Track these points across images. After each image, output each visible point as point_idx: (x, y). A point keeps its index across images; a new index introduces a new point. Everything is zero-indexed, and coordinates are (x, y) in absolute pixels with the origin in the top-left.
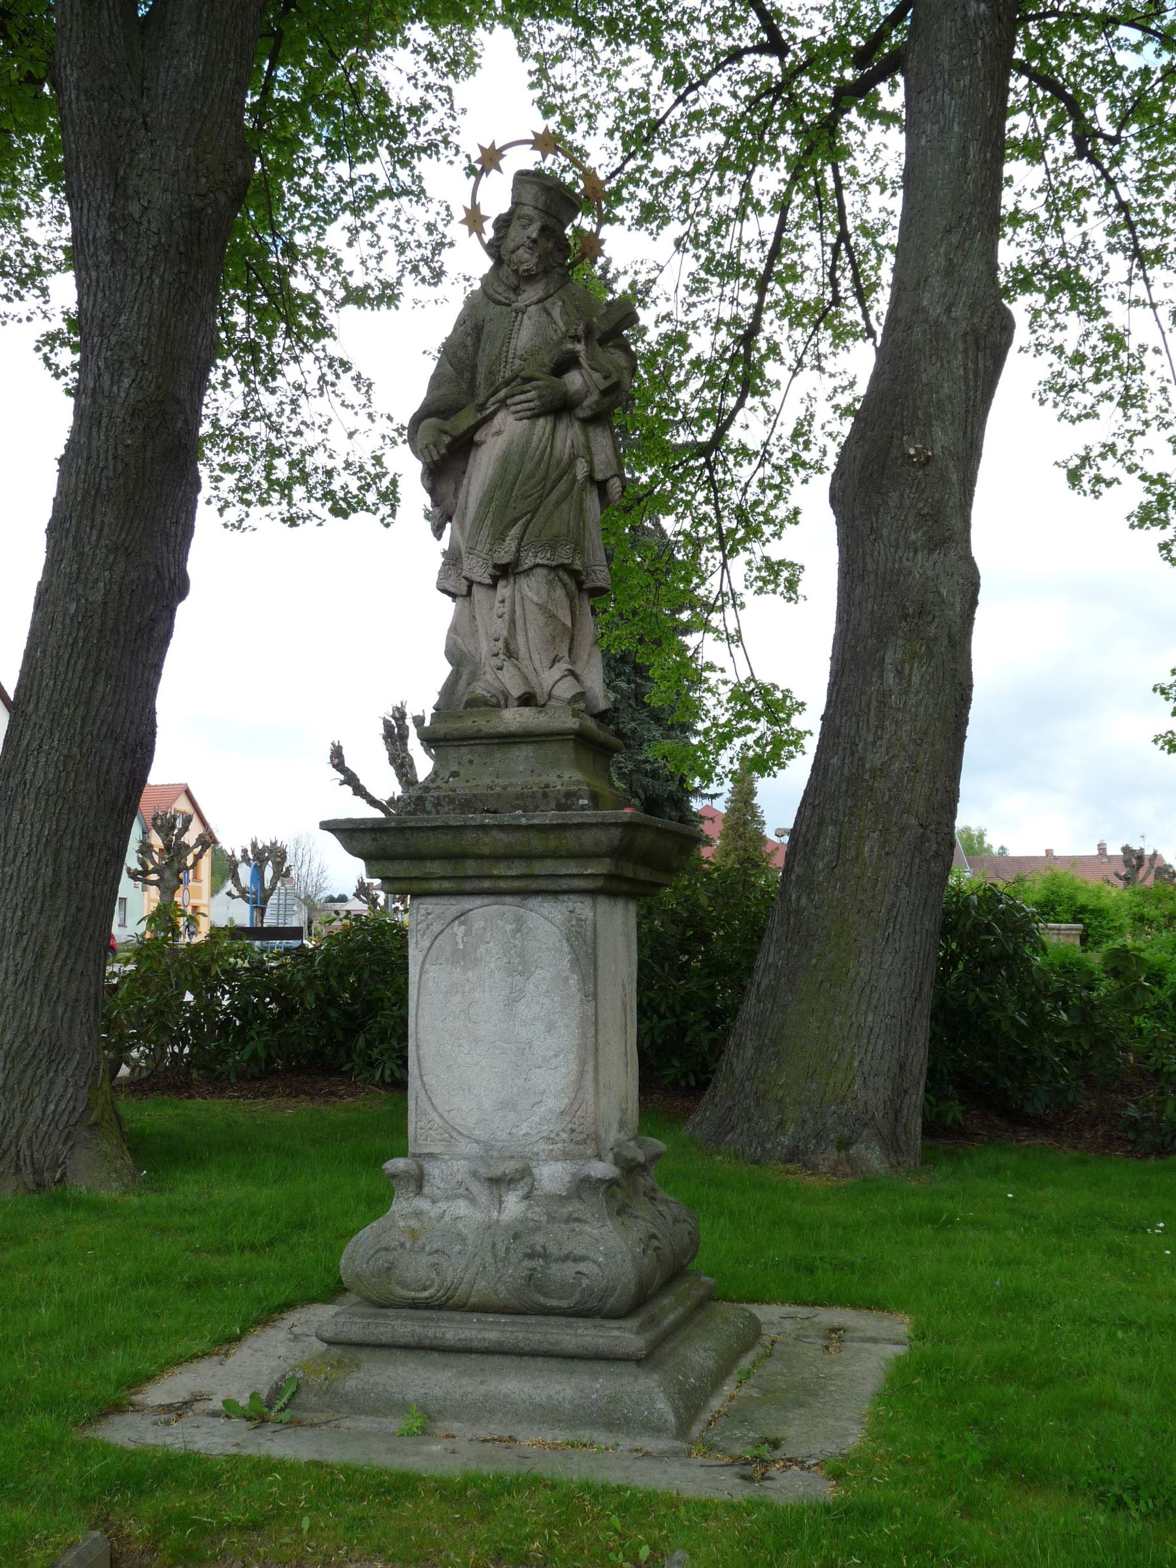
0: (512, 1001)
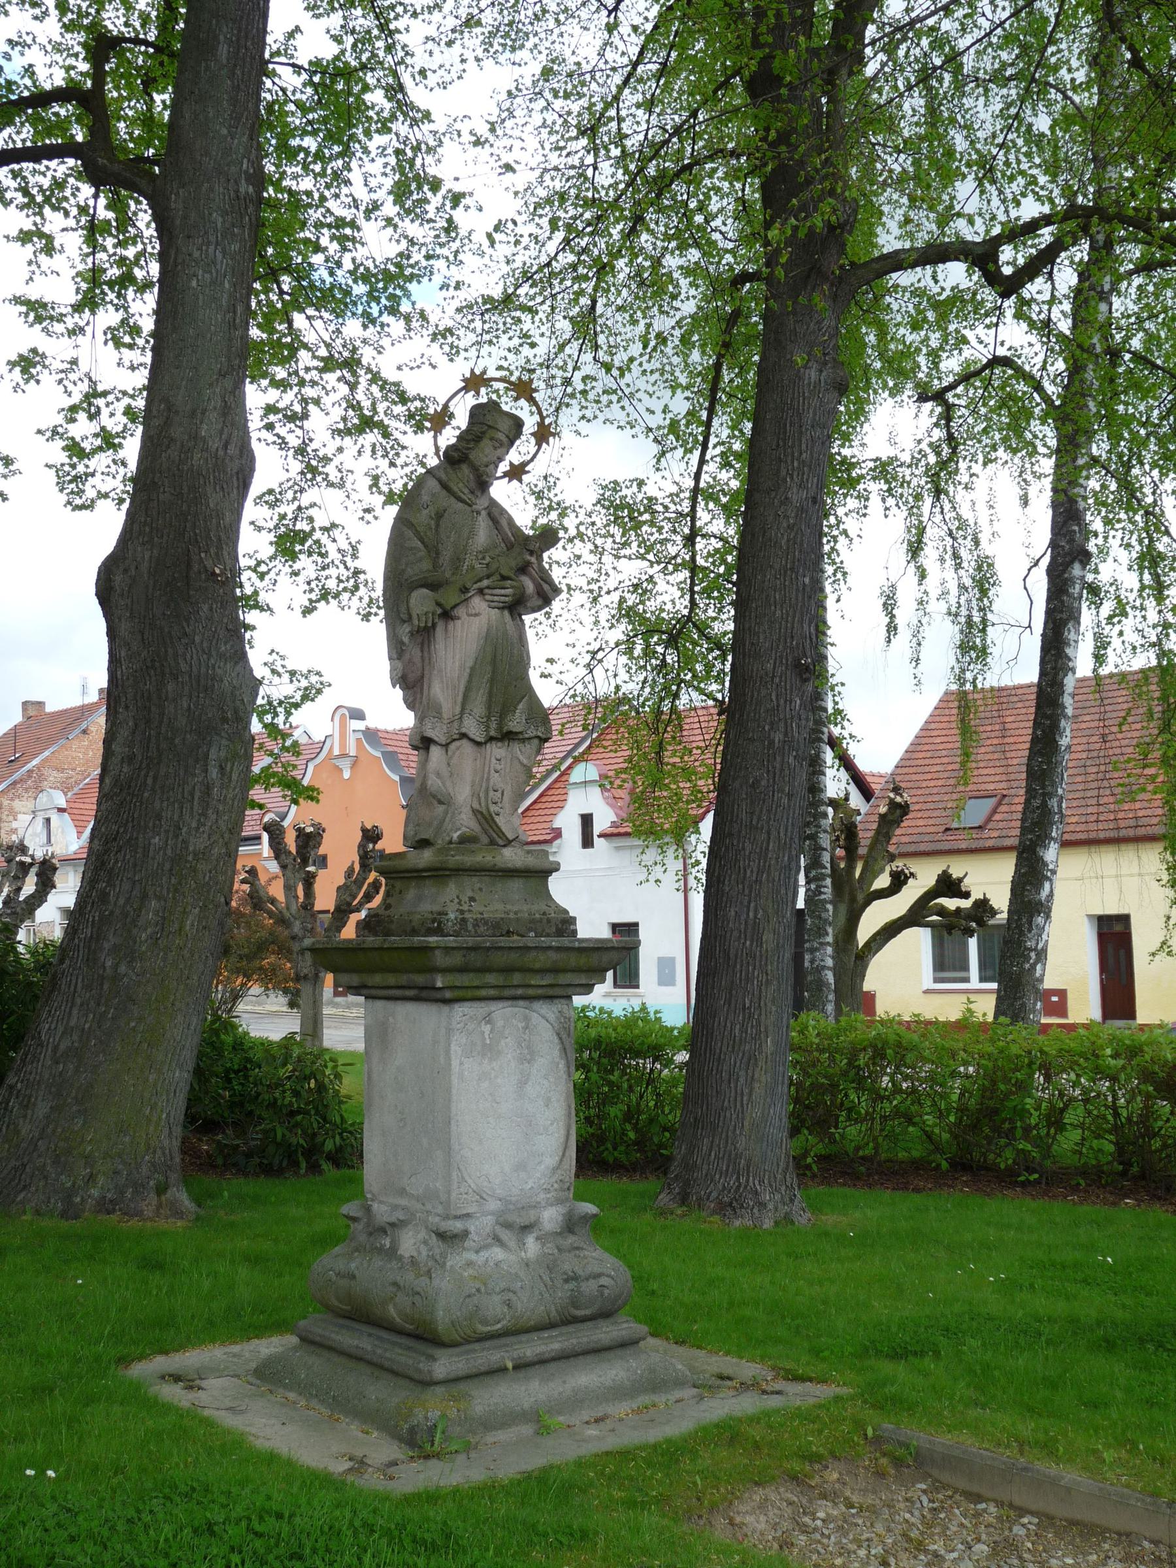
0: (523, 1083)
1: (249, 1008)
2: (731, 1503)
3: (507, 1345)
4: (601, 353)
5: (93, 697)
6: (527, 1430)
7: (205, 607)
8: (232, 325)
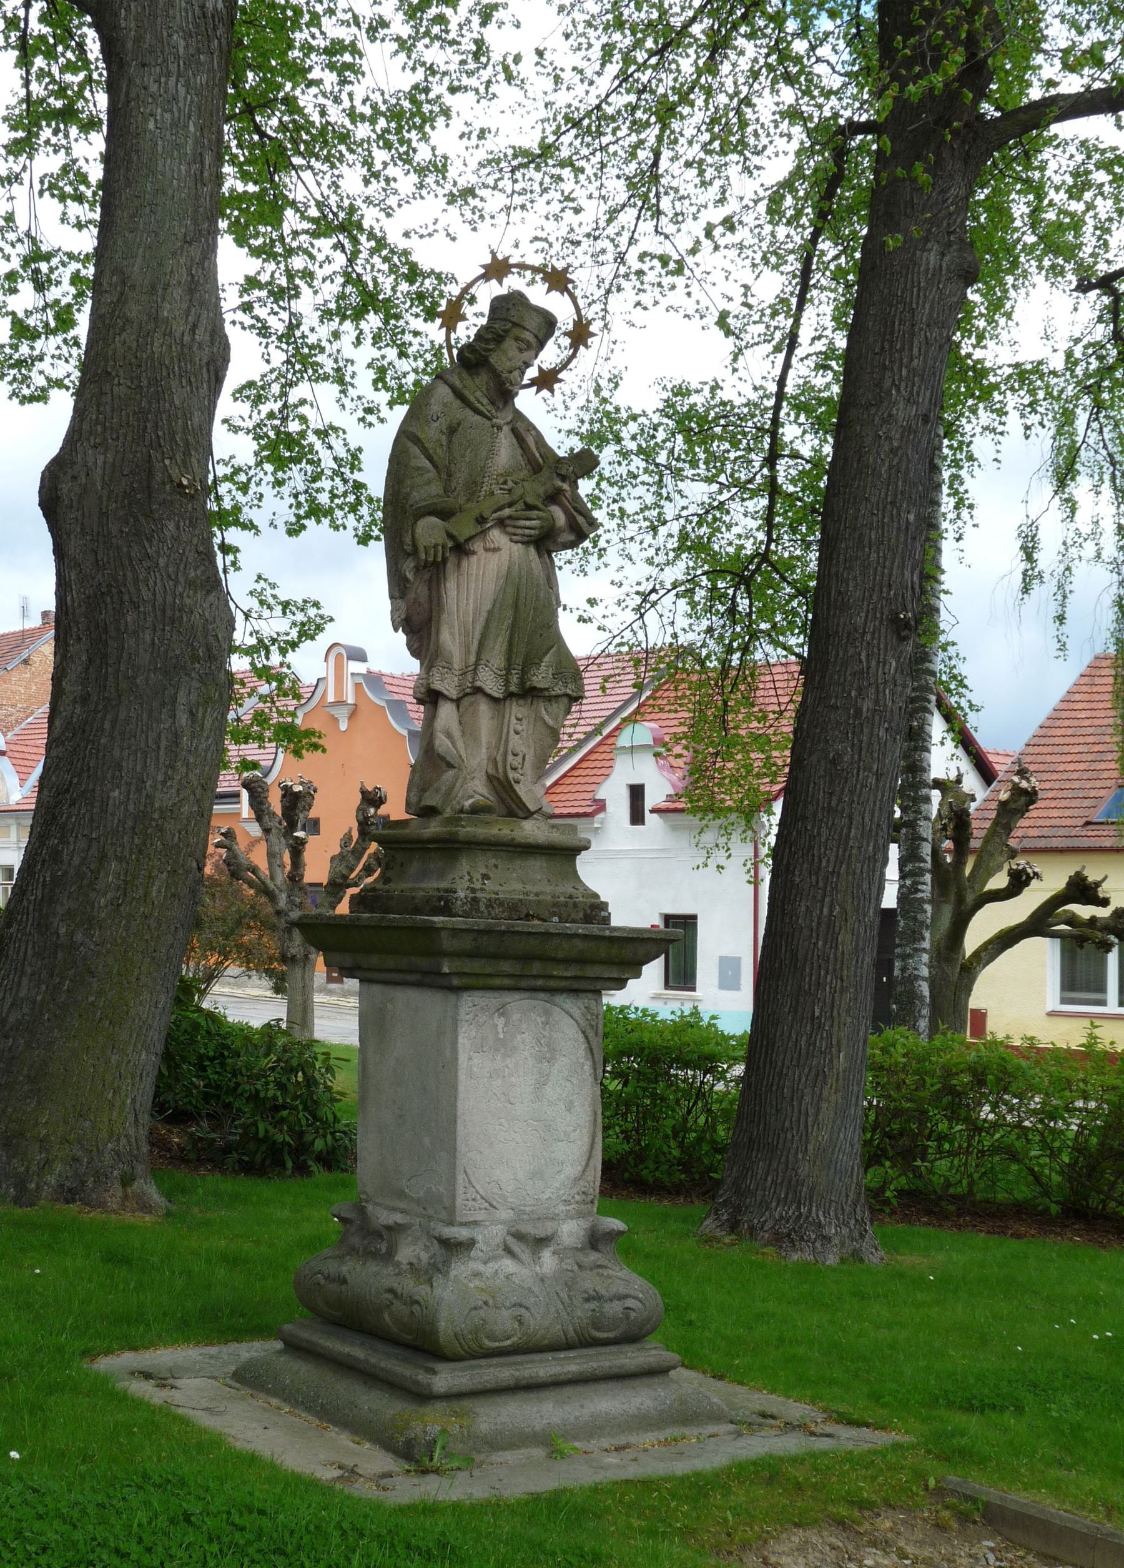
0: (541, 1084)
1: (226, 990)
2: (765, 1541)
3: (518, 1364)
4: (664, 220)
5: (35, 622)
6: (538, 1453)
7: (171, 526)
8: (199, 179)
